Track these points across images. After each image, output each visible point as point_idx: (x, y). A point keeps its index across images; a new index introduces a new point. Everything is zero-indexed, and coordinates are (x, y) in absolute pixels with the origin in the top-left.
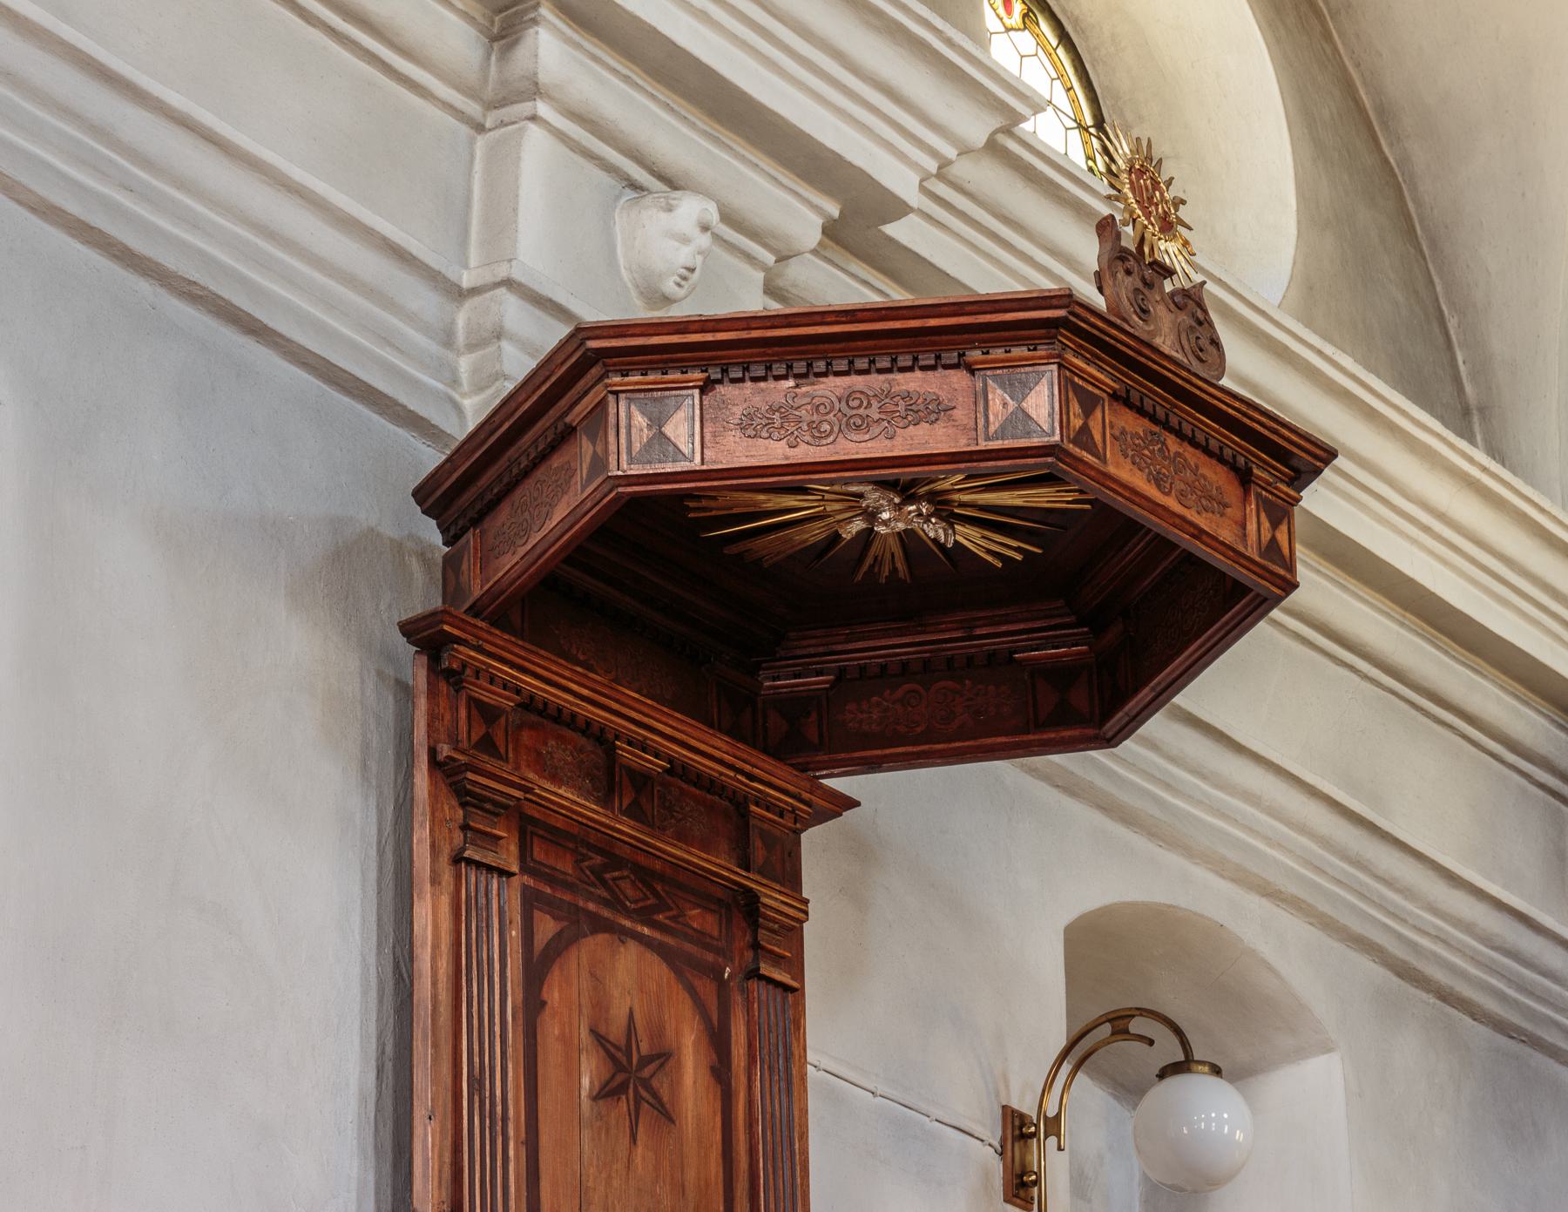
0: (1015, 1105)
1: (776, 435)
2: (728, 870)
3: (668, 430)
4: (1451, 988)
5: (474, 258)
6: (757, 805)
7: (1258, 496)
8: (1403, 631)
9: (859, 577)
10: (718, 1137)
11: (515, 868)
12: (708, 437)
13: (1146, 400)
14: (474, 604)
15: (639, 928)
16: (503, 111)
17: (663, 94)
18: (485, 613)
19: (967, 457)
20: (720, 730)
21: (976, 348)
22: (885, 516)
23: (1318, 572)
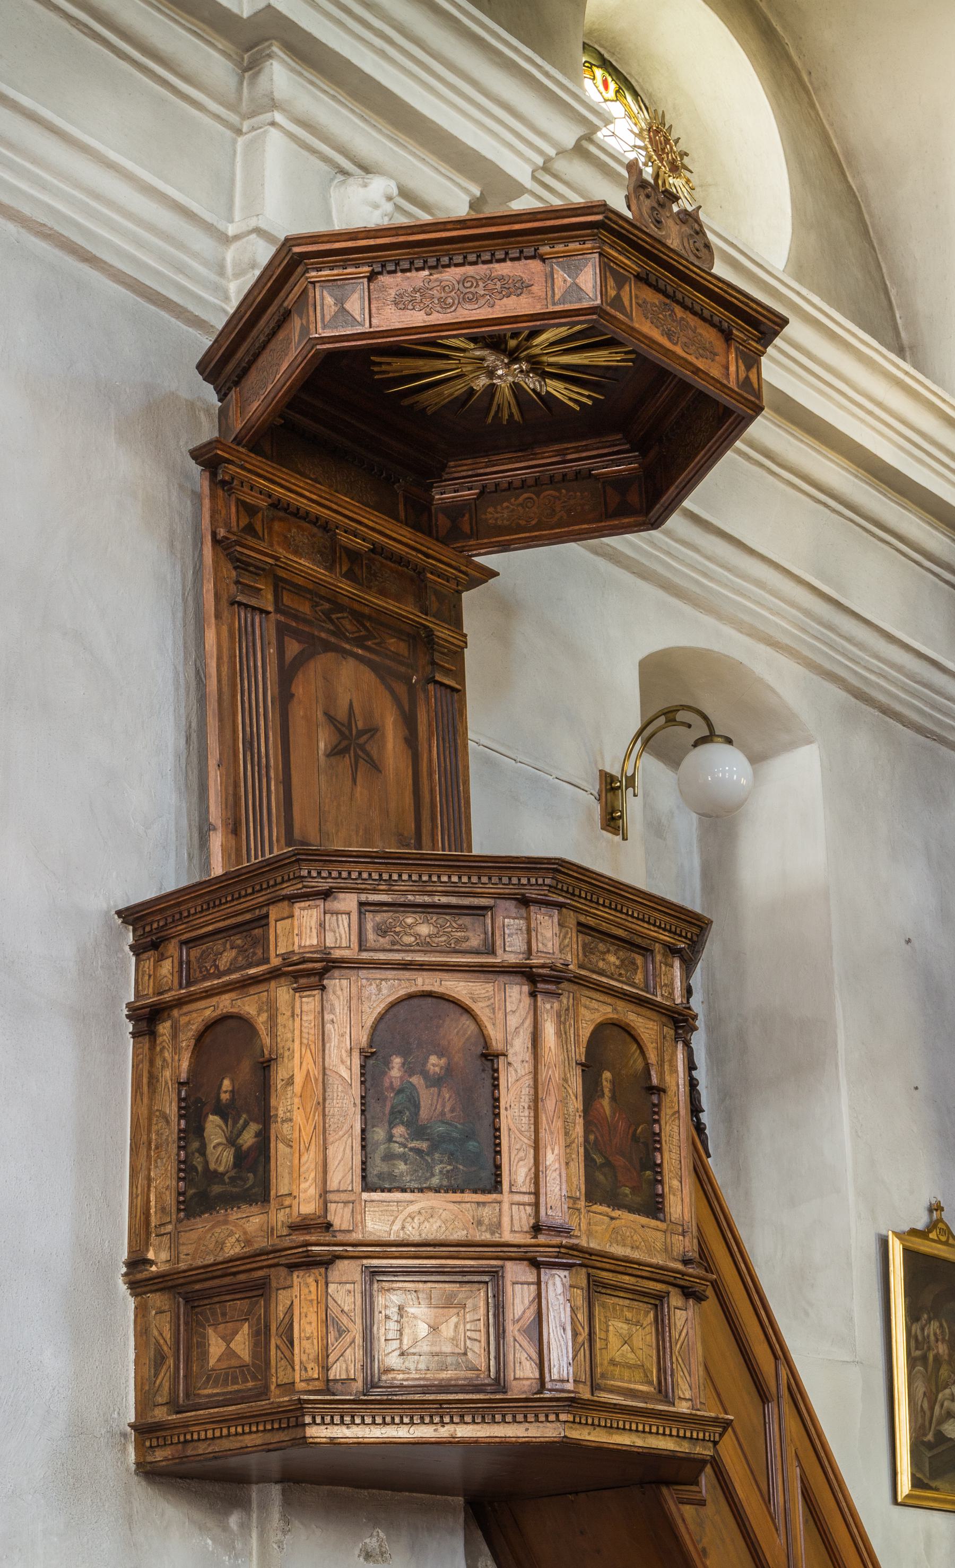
0: (608, 769)
1: (417, 308)
3: (347, 306)
6: (432, 573)
7: (737, 349)
8: (856, 480)
9: (490, 420)
10: (410, 781)
12: (374, 310)
15: (355, 650)
17: (358, 108)
18: (244, 441)
19: (541, 317)
20: (407, 524)
21: (545, 244)
22: (500, 372)
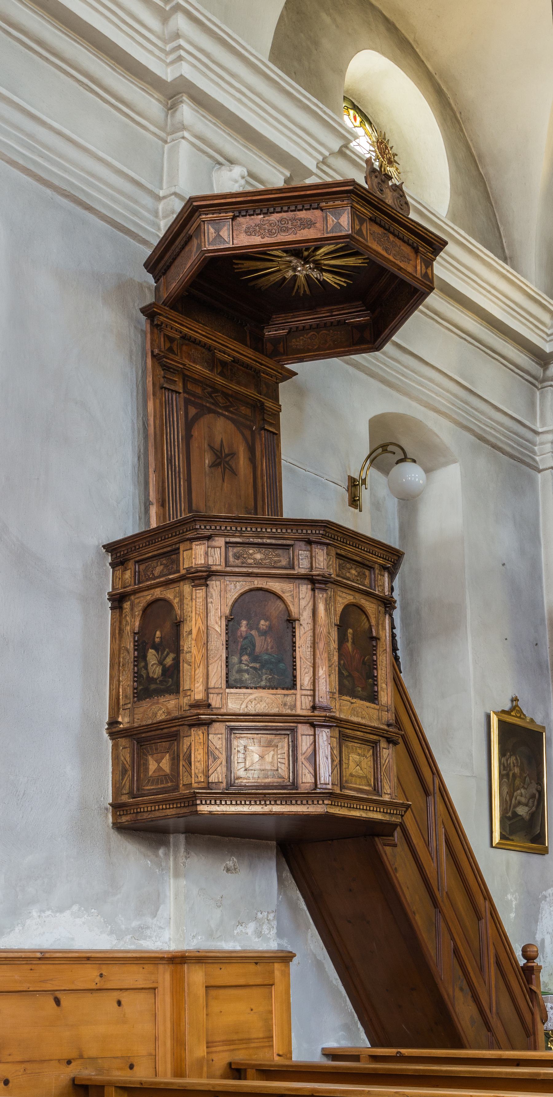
0: (352, 476)
1: (257, 234)
2: (254, 394)
3: (221, 233)
4: (496, 444)
5: (165, 186)
6: (263, 373)
7: (421, 257)
9: (294, 294)
10: (252, 480)
11: (181, 391)
12: (235, 235)
13: (382, 221)
14: (164, 301)
15: (224, 412)
16: (173, 136)
18: (168, 304)
22: (299, 269)
23: (454, 306)
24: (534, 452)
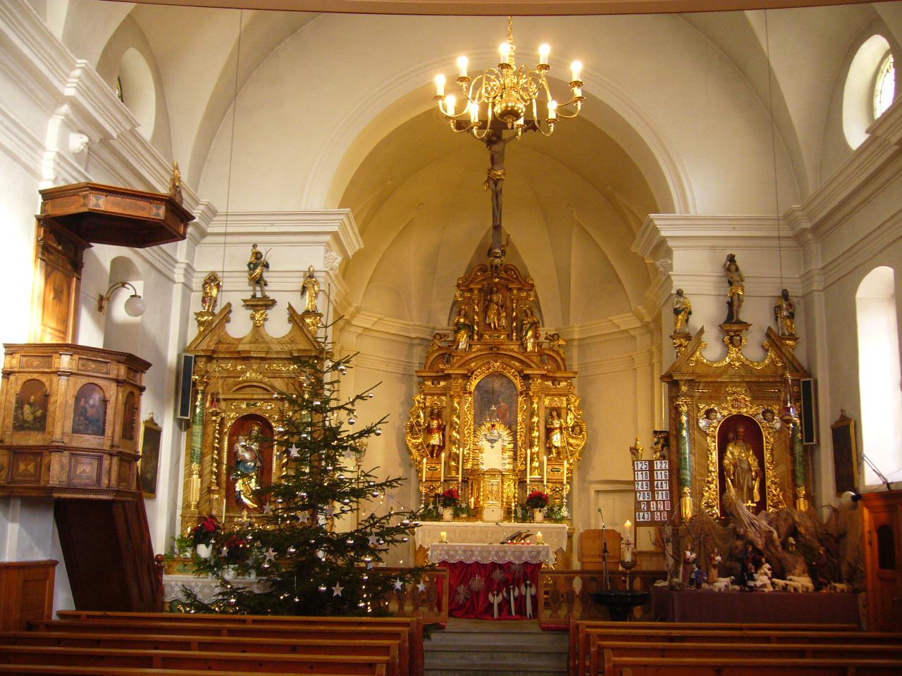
24: (173, 272)
